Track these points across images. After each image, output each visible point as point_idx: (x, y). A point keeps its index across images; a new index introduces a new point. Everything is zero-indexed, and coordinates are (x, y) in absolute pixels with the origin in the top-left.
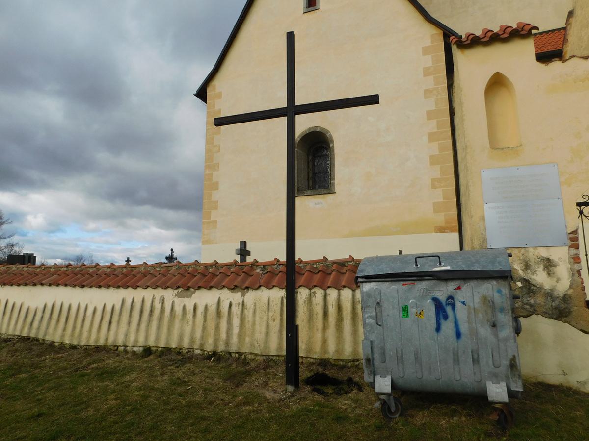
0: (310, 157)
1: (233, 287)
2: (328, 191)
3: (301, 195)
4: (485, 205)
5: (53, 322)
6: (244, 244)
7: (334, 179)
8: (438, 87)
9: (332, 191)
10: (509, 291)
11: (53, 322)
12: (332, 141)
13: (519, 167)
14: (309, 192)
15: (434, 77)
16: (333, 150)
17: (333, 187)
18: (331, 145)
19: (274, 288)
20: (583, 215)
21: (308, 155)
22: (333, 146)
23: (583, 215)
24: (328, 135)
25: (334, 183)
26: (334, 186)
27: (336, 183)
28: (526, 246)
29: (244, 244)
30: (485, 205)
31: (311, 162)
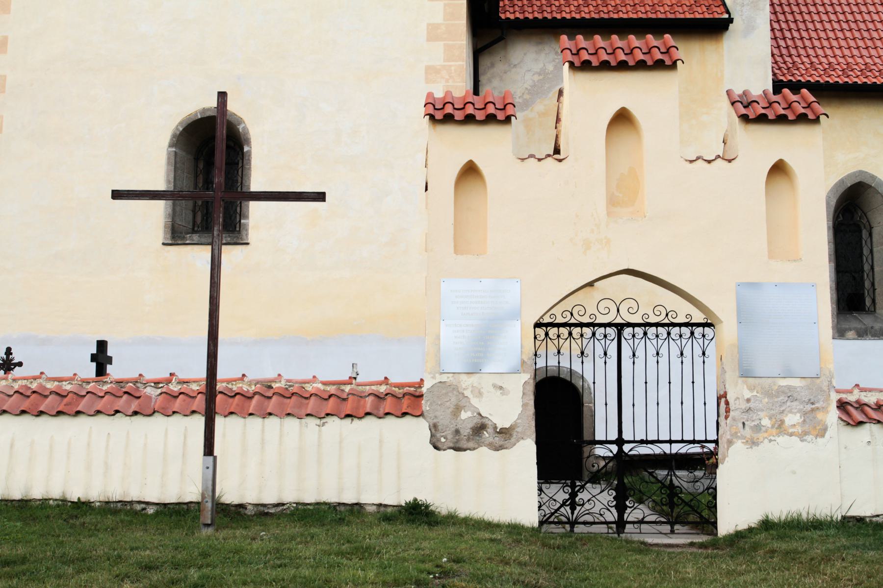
0: (201, 166)
1: (113, 413)
2: (235, 240)
3: (180, 242)
4: (442, 321)
5: (676, 380)
6: (102, 345)
7: (247, 217)
8: (451, 66)
9: (242, 239)
10: (50, 389)
11: (676, 380)
12: (248, 141)
13: (481, 280)
14: (196, 237)
15: (444, 44)
16: (249, 160)
17: (244, 233)
18: (246, 149)
19: (175, 414)
20: (572, 338)
21: (196, 159)
22: (249, 152)
23: (572, 338)
24: (241, 128)
25: (246, 225)
26: (247, 230)
27: (250, 225)
28: (518, 372)
29: (102, 345)
30: (442, 321)
31: (201, 176)
